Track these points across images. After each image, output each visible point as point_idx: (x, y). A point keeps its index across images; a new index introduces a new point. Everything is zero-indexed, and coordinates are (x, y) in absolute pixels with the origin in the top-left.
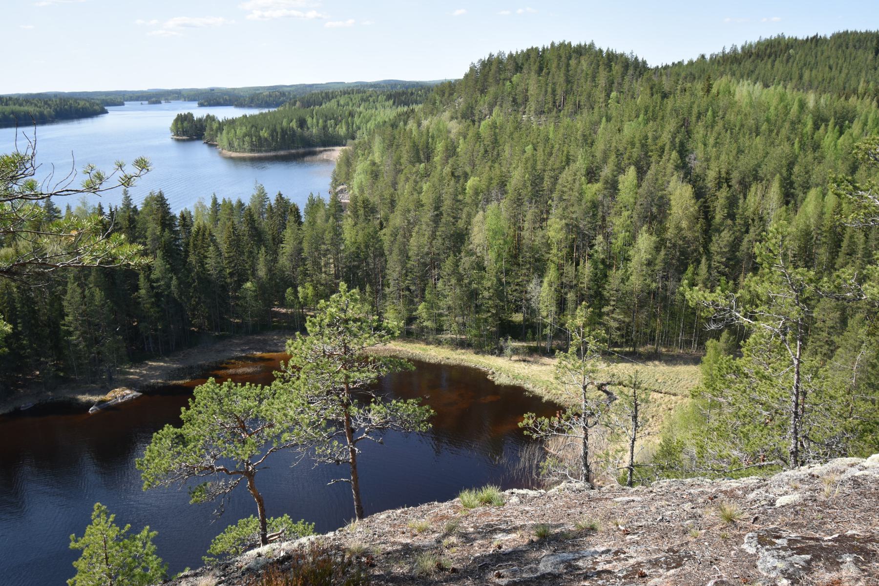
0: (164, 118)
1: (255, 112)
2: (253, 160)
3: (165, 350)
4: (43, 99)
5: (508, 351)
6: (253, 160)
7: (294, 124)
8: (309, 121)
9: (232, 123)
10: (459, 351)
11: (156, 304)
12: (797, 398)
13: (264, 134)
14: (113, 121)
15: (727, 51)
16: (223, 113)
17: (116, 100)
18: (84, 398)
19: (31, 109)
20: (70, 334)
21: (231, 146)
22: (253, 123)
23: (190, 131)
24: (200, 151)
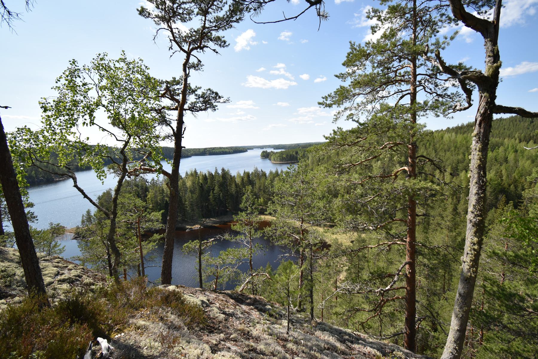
0: (259, 152)
1: (283, 150)
2: (280, 164)
3: (216, 215)
4: (231, 148)
5: (322, 225)
6: (280, 164)
7: (294, 153)
8: (299, 152)
9: (277, 153)
10: (270, 220)
11: (214, 201)
12: (108, 250)
13: (284, 156)
14: (249, 153)
15: (460, 125)
16: (276, 151)
17: (251, 148)
18: (187, 227)
19: (227, 150)
20: (187, 207)
21: (274, 160)
22: (282, 153)
23: (266, 156)
24: (268, 161)
